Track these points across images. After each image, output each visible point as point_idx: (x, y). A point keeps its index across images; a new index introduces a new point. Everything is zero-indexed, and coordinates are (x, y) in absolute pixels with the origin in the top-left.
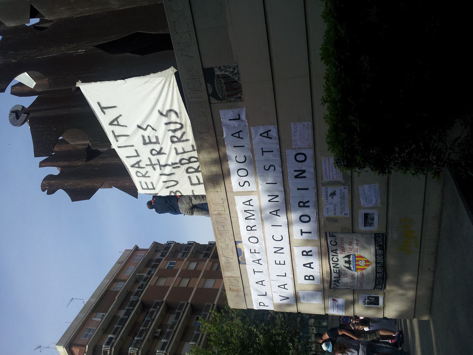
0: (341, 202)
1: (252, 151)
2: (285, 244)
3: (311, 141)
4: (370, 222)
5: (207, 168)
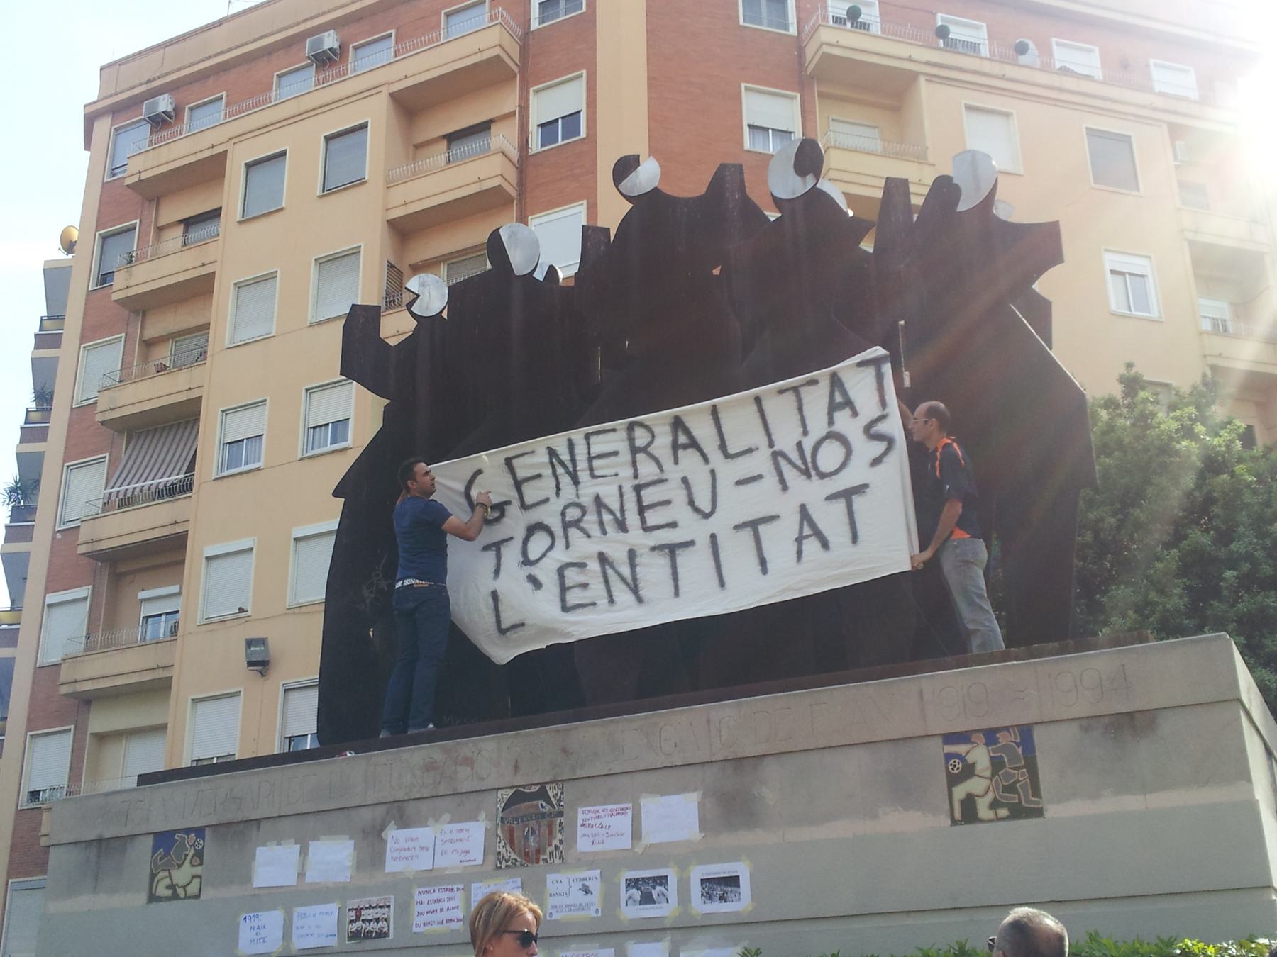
4: (715, 892)
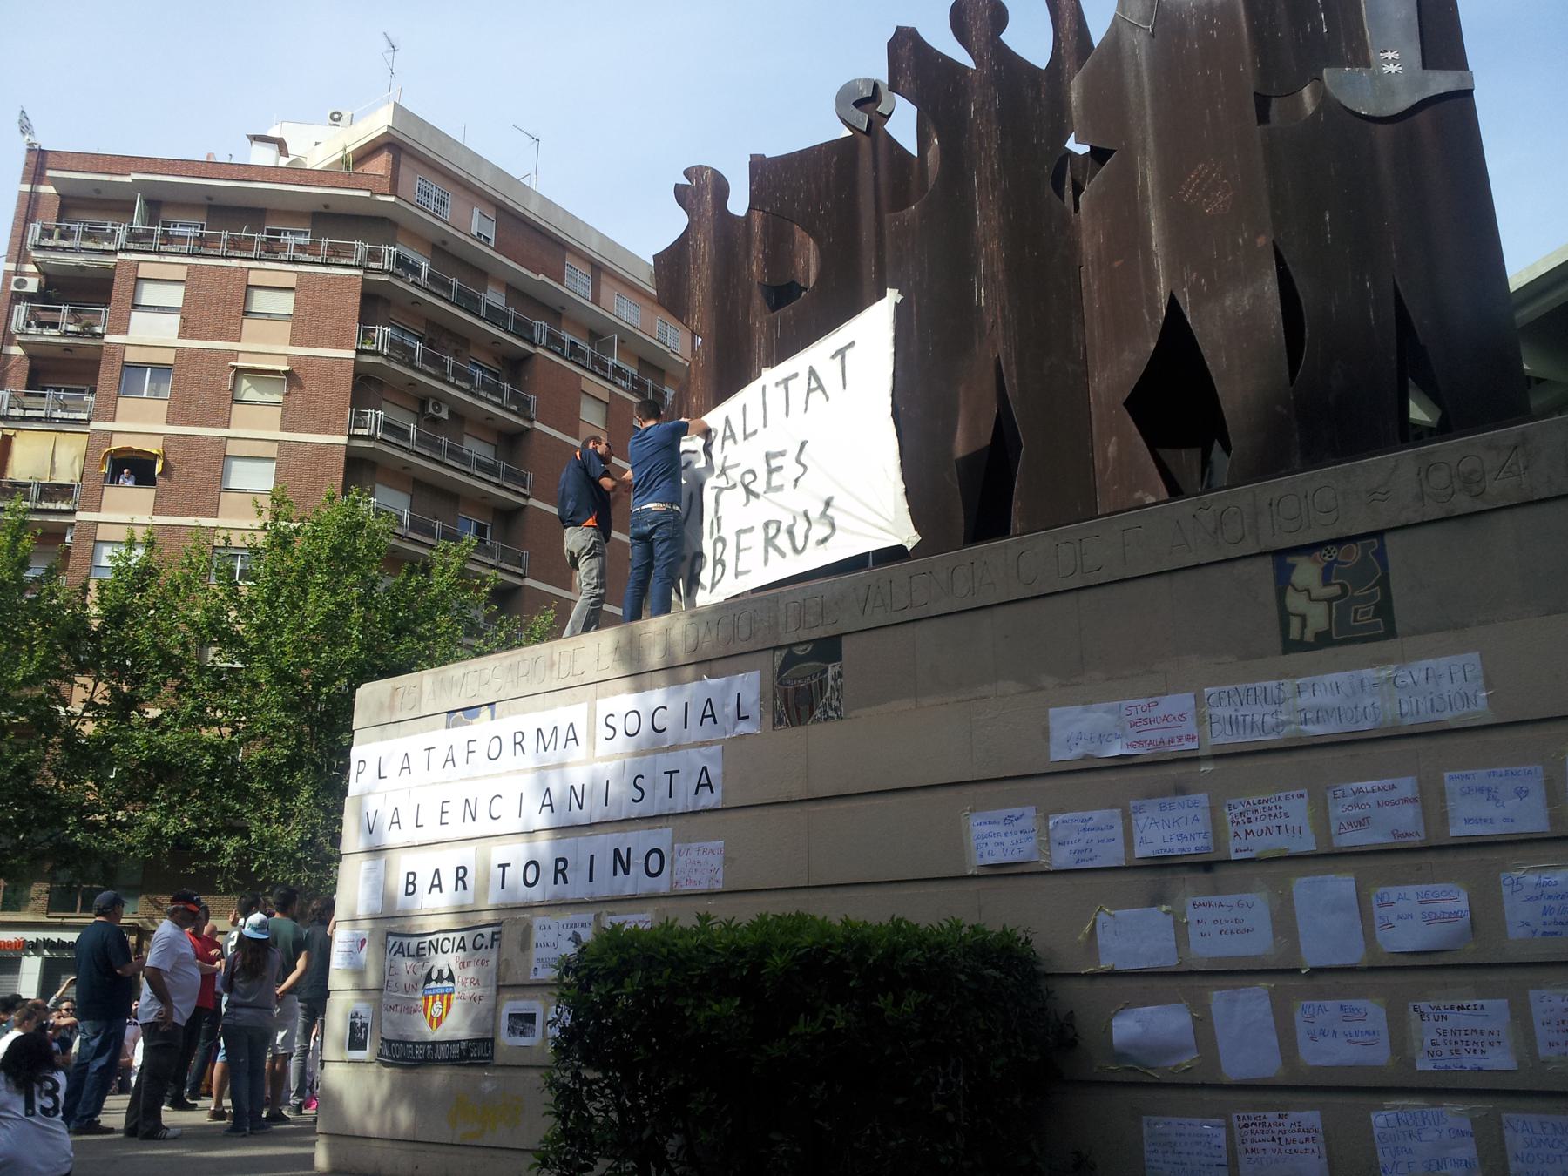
1: (673, 748)
2: (484, 826)
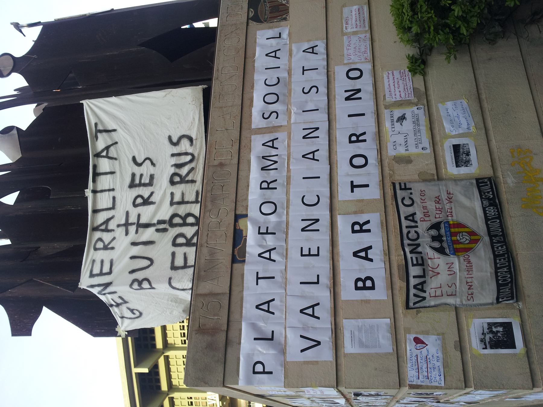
0: (415, 129)
3: (369, 54)
4: (464, 159)
5: (221, 98)
